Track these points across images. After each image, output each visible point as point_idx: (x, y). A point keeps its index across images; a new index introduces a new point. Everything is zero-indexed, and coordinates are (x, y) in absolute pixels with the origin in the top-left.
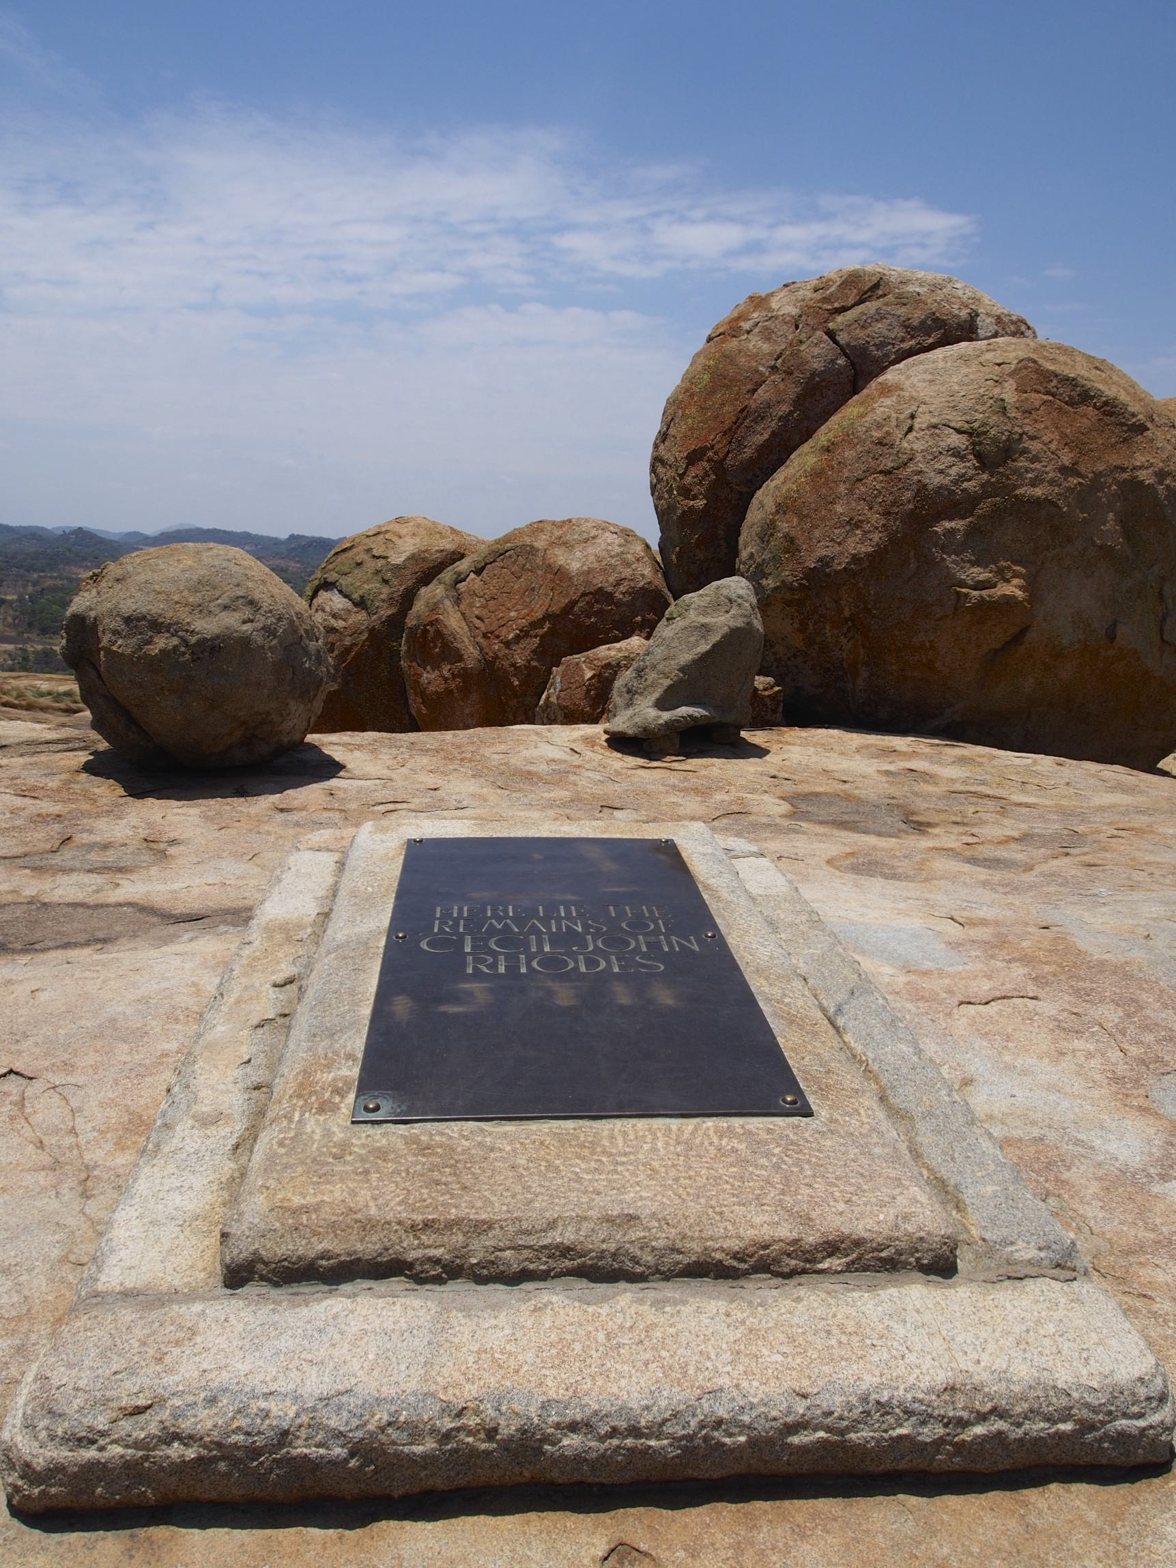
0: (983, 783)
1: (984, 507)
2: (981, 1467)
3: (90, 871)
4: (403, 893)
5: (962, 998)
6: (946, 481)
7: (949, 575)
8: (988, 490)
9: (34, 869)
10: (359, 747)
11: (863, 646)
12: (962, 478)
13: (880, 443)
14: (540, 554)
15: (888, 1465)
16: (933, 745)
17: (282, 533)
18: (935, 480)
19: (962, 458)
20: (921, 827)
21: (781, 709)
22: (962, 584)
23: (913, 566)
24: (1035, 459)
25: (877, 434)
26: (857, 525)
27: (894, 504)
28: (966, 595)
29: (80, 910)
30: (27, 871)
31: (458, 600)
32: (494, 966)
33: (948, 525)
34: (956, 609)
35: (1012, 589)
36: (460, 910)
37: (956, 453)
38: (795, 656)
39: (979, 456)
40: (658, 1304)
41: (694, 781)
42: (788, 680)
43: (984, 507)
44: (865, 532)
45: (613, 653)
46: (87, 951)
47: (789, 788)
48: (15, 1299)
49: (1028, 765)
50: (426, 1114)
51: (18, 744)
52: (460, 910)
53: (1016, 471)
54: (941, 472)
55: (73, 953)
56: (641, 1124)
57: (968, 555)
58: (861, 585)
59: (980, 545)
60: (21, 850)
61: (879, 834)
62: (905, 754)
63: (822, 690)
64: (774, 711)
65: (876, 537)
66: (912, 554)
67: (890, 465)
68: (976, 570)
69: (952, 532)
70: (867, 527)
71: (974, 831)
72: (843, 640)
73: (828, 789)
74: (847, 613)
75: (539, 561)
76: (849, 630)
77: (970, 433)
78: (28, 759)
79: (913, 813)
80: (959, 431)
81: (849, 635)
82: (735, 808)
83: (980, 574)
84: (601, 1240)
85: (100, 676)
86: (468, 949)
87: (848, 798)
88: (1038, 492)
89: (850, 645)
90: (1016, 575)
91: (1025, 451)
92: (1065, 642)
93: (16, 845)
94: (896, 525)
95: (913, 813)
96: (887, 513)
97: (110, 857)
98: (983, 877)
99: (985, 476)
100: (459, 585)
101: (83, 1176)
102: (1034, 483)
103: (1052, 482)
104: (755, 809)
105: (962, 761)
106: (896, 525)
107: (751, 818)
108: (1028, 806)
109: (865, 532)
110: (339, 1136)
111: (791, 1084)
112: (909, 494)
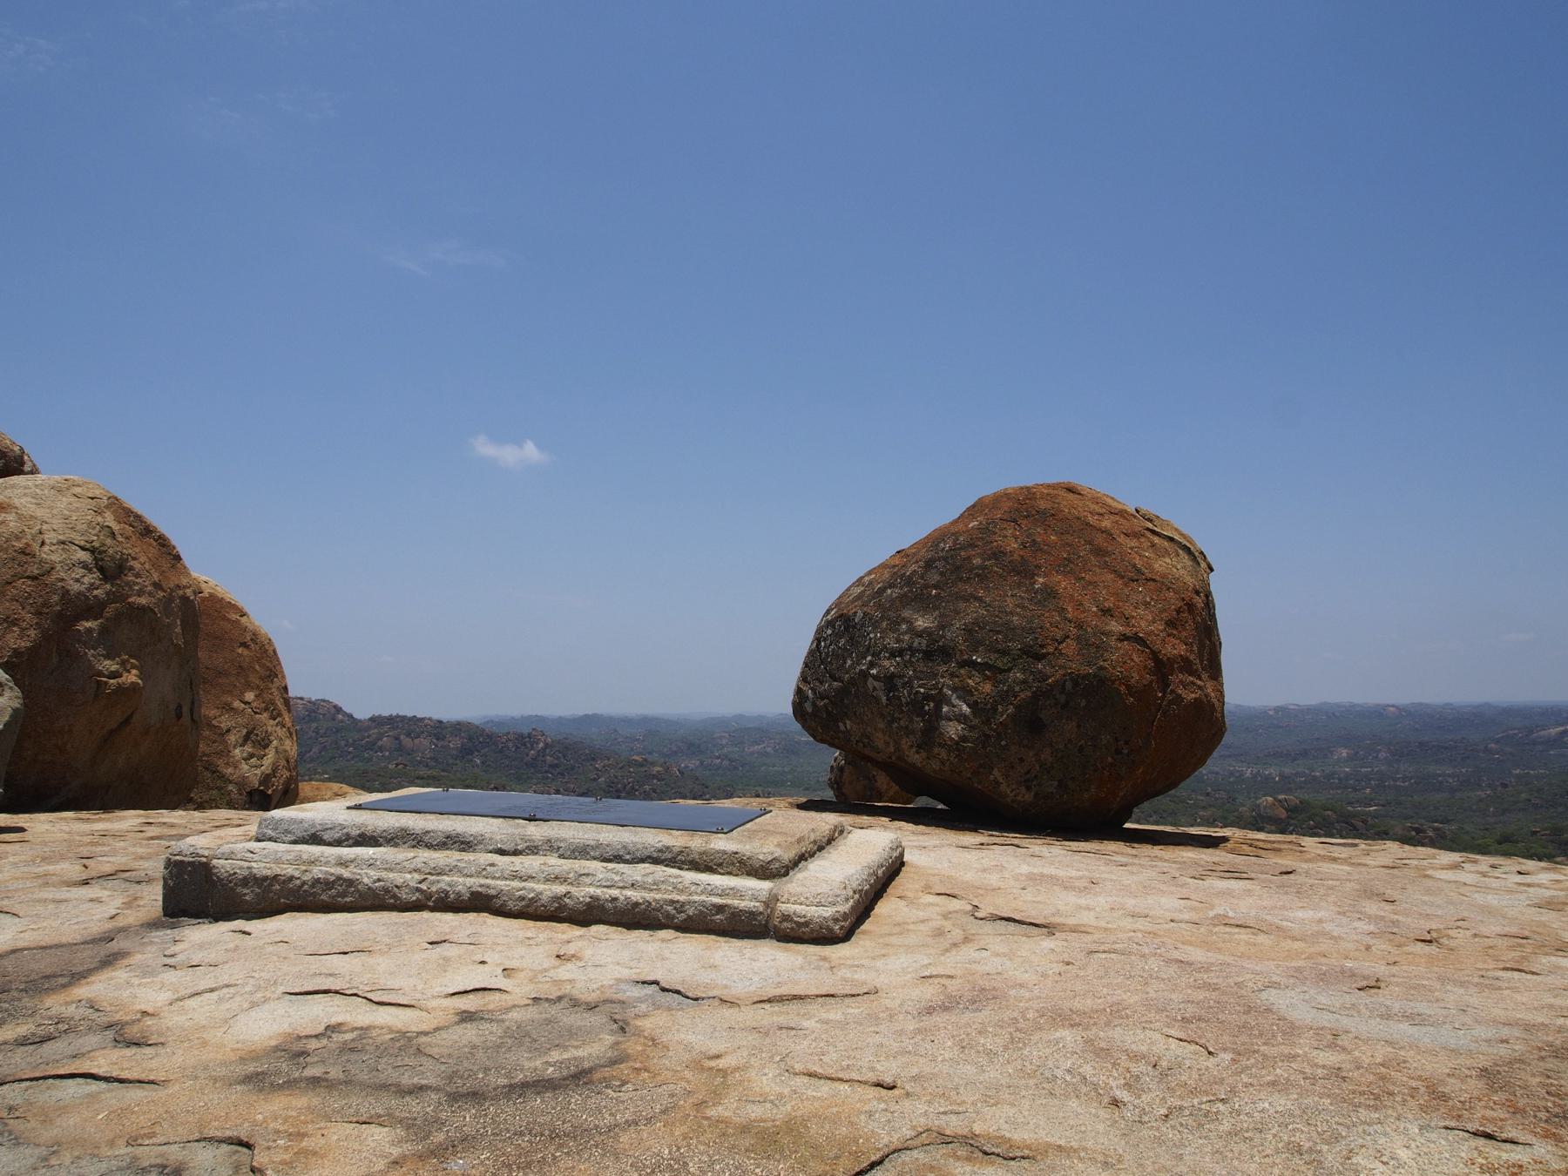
1: (110, 611)
6: (83, 588)
7: (91, 667)
8: (113, 597)
12: (92, 587)
13: (23, 552)
18: (76, 587)
19: (90, 570)
22: (100, 674)
24: (138, 575)
25: (18, 545)
26: (14, 623)
27: (44, 605)
33: (88, 624)
35: (132, 677)
37: (85, 566)
39: (101, 569)
43: (110, 611)
44: (23, 630)
50: (1332, 836)
53: (127, 583)
54: (77, 580)
57: (100, 650)
59: (109, 642)
65: (32, 633)
68: (107, 662)
69: (90, 630)
70: (24, 625)
77: (93, 551)
80: (83, 548)
83: (111, 665)
88: (143, 601)
90: (134, 667)
91: (131, 568)
93: (63, 1110)
94: (47, 624)
96: (38, 613)
98: (521, 934)
99: (108, 586)
102: (140, 593)
103: (150, 594)
106: (47, 624)
109: (23, 630)
112: (56, 598)
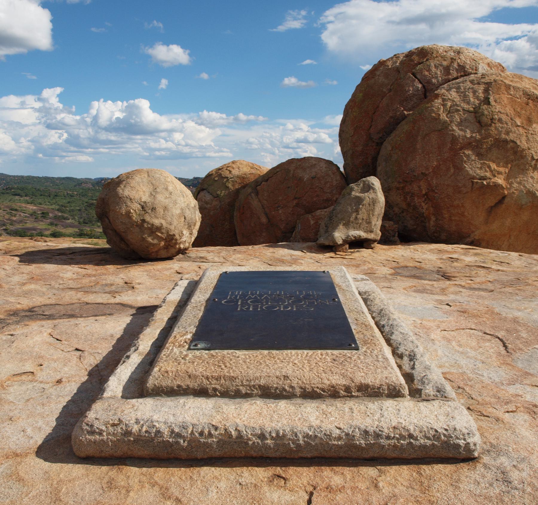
0: (484, 262)
2: (405, 456)
3: (105, 293)
4: (216, 287)
5: (442, 329)
9: (84, 292)
10: (212, 251)
11: (432, 207)
14: (292, 172)
15: (371, 454)
16: (463, 248)
17: (191, 177)
20: (448, 278)
21: (396, 235)
23: (452, 171)
28: (477, 182)
29: (101, 305)
30: (82, 293)
31: (257, 194)
32: (249, 308)
34: (472, 189)
36: (239, 293)
38: (403, 212)
40: (295, 405)
41: (354, 262)
42: (400, 223)
45: (323, 213)
46: (104, 317)
47: (395, 264)
48: (77, 409)
49: (506, 256)
51: (79, 252)
52: (239, 293)
55: (97, 318)
56: (294, 352)
58: (429, 179)
60: (79, 286)
61: (430, 280)
62: (450, 252)
63: (415, 227)
64: (394, 236)
66: (451, 166)
67: (440, 128)
71: (472, 279)
72: (423, 204)
73: (411, 265)
74: (424, 192)
75: (291, 175)
76: (425, 200)
78: (83, 256)
79: (447, 273)
81: (426, 202)
82: (369, 271)
84: (274, 383)
85: (110, 222)
86: (239, 304)
87: (420, 268)
89: (426, 206)
92: (523, 203)
95: (447, 273)
97: (113, 288)
100: (258, 187)
101: (100, 378)
104: (377, 272)
105: (476, 254)
107: (376, 275)
108: (502, 271)
110: (185, 353)
111: (354, 341)
